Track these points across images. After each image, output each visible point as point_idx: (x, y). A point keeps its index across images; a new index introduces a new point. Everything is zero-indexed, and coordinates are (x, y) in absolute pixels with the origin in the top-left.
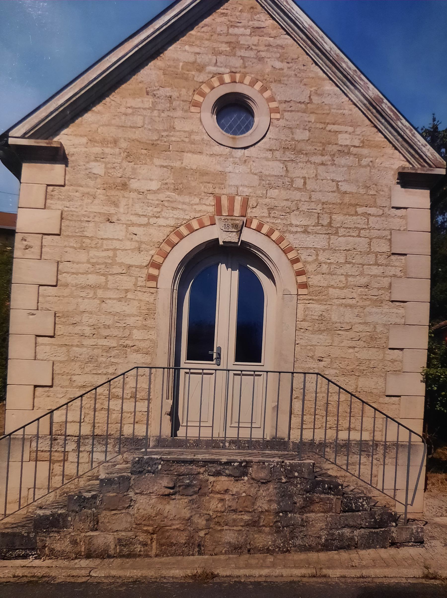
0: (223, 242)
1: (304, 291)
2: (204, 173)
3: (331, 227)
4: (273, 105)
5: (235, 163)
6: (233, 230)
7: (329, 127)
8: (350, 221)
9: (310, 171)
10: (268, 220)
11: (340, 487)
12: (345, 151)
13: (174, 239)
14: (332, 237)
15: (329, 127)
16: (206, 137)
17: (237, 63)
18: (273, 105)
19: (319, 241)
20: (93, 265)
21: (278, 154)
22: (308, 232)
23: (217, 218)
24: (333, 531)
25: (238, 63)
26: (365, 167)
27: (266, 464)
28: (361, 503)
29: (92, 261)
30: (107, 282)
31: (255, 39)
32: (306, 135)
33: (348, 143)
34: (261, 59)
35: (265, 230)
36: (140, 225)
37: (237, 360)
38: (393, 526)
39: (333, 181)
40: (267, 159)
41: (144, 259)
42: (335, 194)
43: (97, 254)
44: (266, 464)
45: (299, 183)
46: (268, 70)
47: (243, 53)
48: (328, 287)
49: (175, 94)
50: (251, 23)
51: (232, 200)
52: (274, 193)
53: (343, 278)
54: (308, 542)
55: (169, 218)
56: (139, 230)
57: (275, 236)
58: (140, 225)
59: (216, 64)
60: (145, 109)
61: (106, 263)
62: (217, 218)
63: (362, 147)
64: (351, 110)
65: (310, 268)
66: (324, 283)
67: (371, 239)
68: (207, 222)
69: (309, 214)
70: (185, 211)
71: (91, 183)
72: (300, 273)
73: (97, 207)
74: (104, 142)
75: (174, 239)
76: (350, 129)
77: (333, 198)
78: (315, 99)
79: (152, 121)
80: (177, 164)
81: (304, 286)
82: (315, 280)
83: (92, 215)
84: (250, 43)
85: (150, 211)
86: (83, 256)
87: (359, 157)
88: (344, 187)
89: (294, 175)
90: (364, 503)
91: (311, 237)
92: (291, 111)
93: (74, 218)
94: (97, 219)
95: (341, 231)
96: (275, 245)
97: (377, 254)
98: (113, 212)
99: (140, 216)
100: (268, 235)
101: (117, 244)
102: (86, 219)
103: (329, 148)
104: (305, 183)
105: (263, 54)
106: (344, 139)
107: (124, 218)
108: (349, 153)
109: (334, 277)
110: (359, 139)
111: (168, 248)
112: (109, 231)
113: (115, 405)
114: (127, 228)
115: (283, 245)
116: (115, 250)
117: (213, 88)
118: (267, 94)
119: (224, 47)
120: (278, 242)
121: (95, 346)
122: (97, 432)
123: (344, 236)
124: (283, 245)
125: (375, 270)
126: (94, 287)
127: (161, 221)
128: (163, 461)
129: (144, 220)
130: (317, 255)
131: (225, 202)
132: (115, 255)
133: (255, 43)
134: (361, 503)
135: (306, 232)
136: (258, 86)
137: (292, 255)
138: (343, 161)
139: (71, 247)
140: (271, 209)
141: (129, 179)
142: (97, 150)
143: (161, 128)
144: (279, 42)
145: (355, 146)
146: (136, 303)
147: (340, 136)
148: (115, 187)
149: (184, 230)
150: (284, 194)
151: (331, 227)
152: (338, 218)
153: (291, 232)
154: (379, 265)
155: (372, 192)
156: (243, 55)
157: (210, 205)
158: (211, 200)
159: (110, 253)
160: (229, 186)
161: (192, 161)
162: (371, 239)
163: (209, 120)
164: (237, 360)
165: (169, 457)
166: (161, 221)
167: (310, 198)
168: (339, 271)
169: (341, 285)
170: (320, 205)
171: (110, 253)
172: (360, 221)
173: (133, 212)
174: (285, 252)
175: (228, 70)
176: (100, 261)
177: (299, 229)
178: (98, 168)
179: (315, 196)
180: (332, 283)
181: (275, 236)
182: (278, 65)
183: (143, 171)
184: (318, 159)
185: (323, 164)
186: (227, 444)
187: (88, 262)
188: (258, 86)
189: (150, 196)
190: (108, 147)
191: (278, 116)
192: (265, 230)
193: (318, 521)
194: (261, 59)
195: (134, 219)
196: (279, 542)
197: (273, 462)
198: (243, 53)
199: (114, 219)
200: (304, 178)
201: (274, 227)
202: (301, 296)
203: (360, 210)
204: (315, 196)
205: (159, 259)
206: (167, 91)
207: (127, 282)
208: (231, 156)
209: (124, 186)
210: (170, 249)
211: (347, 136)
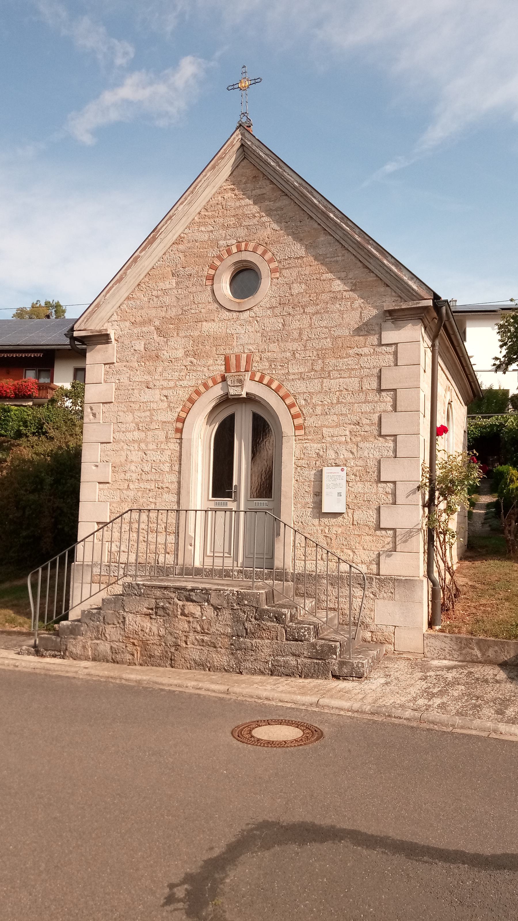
0: (247, 394)
1: (302, 432)
3: (324, 371)
4: (273, 265)
6: (238, 384)
11: (284, 616)
14: (325, 380)
18: (273, 265)
19: (315, 385)
24: (279, 658)
27: (222, 592)
28: (303, 633)
30: (146, 436)
38: (333, 658)
40: (269, 317)
44: (222, 592)
45: (296, 334)
48: (322, 426)
51: (238, 358)
54: (260, 666)
56: (169, 393)
64: (343, 256)
73: (140, 377)
74: (143, 323)
82: (310, 421)
90: (306, 633)
100: (268, 385)
101: (155, 406)
107: (157, 383)
110: (351, 283)
112: (147, 395)
113: (152, 537)
122: (140, 560)
125: (366, 408)
126: (139, 442)
127: (185, 383)
128: (145, 586)
131: (233, 361)
134: (303, 633)
148: (150, 358)
151: (324, 371)
153: (288, 380)
158: (221, 361)
164: (270, 497)
165: (149, 583)
166: (185, 383)
181: (274, 386)
185: (317, 313)
186: (236, 573)
191: (278, 275)
193: (265, 646)
195: (165, 384)
196: (233, 662)
197: (227, 590)
199: (151, 385)
202: (299, 437)
205: (183, 415)
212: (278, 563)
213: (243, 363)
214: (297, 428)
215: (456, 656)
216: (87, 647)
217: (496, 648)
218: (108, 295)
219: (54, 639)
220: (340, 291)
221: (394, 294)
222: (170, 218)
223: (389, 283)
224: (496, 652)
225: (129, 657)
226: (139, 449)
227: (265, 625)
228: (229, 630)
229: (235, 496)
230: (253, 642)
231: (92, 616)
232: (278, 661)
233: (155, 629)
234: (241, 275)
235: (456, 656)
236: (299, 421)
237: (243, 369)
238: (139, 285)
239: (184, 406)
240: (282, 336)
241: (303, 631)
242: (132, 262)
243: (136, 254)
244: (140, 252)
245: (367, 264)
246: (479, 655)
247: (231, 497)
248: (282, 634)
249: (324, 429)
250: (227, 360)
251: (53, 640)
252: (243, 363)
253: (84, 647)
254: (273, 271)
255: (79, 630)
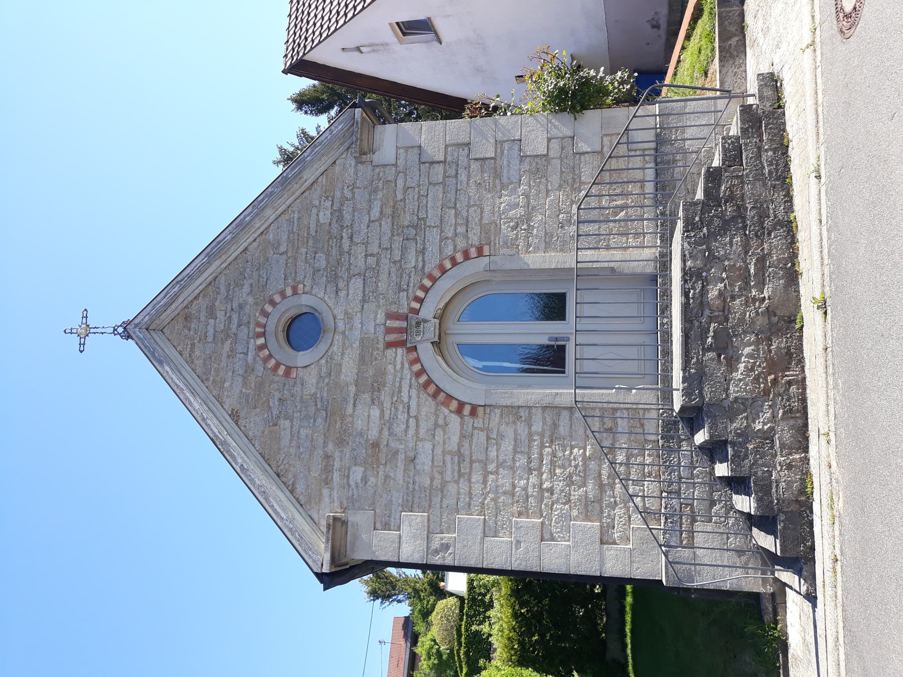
2: (362, 360)
4: (289, 292)
5: (351, 329)
7: (313, 232)
8: (411, 205)
9: (360, 251)
10: (410, 291)
12: (338, 214)
13: (432, 389)
15: (313, 232)
16: (323, 361)
17: (243, 333)
19: (433, 236)
20: (460, 475)
21: (341, 284)
22: (424, 249)
23: (409, 345)
25: (243, 333)
26: (353, 193)
29: (456, 478)
30: (479, 461)
31: (220, 315)
32: (321, 256)
33: (328, 213)
34: (241, 307)
35: (421, 294)
36: (417, 425)
37: (564, 319)
39: (368, 226)
41: (454, 420)
42: (383, 223)
43: (449, 473)
46: (251, 300)
47: (234, 326)
48: (481, 225)
49: (277, 395)
50: (202, 319)
51: (389, 331)
52: (382, 286)
53: (472, 210)
55: (410, 393)
57: (427, 283)
58: (417, 425)
59: (246, 354)
60: (292, 428)
61: (459, 462)
62: (409, 345)
63: (333, 197)
64: (294, 212)
65: (461, 244)
66: (477, 229)
67: (430, 184)
68: (413, 355)
69: (404, 250)
70: (401, 379)
71: (372, 480)
72: (467, 256)
74: (328, 469)
75: (432, 389)
76: (314, 211)
77: (386, 225)
78: (282, 249)
79: (307, 417)
80: (353, 389)
81: (480, 253)
82: (474, 239)
83: (407, 479)
84: (223, 319)
85: (402, 417)
86: (452, 488)
87: (344, 199)
88: (375, 213)
89: (363, 267)
91: (427, 246)
92: (296, 273)
93: (410, 498)
94: (412, 474)
95: (421, 215)
96: (438, 283)
97: (445, 177)
98: (403, 456)
99: (407, 427)
100: (426, 290)
101: (439, 451)
102: (411, 486)
103: (335, 231)
104: (371, 255)
105: (235, 305)
106: (325, 217)
108: (340, 211)
109: (470, 219)
111: (442, 395)
112: (425, 461)
114: (421, 440)
115: (437, 273)
116: (444, 453)
117: (270, 356)
118: (277, 298)
119: (227, 346)
120: (434, 280)
121: (552, 474)
123: (427, 211)
124: (437, 273)
127: (413, 404)
129: (412, 422)
130: (447, 238)
131: (392, 337)
132: (450, 452)
133: (223, 313)
135: (423, 252)
136: (269, 308)
137: (448, 265)
138: (347, 217)
139: (441, 501)
140: (400, 290)
141: (367, 440)
142: (336, 476)
143: (314, 408)
144: (223, 289)
145: (332, 205)
146: (503, 427)
147: (322, 221)
149: (423, 379)
150: (384, 276)
152: (407, 219)
154: (457, 173)
155: (380, 185)
156: (235, 326)
157: (396, 353)
158: (390, 352)
159: (448, 458)
160: (375, 333)
161: (349, 370)
162: (430, 184)
163: (302, 358)
164: (564, 319)
167: (387, 249)
168: (465, 214)
169: (479, 211)
170: (395, 238)
171: (448, 458)
172: (412, 195)
173: (404, 434)
174: (444, 271)
175: (252, 340)
176: (457, 469)
177: (420, 259)
178: (357, 473)
179: (386, 244)
180: (477, 220)
181: (427, 283)
182: (246, 289)
183: (359, 424)
184: (346, 243)
185: (351, 238)
187: (457, 482)
188: (269, 308)
189: (387, 417)
190: (333, 465)
191: (301, 286)
192: (421, 294)
194: (241, 307)
195: (411, 432)
198: (234, 326)
199: (411, 454)
200: (366, 256)
201: (419, 285)
203: (400, 196)
204: (386, 244)
205: (454, 405)
206: (274, 403)
207: (480, 438)
208: (343, 333)
209: (376, 445)
210: (442, 394)
211: (321, 214)
212: (650, 269)
213: (396, 324)
214: (480, 253)
215: (741, 61)
216: (788, 461)
217: (726, 23)
218: (283, 515)
219: (782, 525)
220: (331, 213)
221: (344, 156)
222: (204, 419)
223: (330, 161)
224: (730, 24)
225: (793, 389)
226: (496, 473)
227: (725, 192)
228: (737, 239)
229: (563, 339)
230: (749, 206)
231: (739, 456)
232: (770, 172)
233: (748, 350)
234: (291, 334)
235: (741, 61)
236: (473, 252)
237: (404, 324)
238: (278, 475)
239: (443, 404)
240: (369, 275)
241: (727, 146)
242: (246, 475)
243: (238, 470)
244: (237, 463)
245: (307, 184)
246: (737, 38)
247: (564, 346)
248: (734, 171)
249: (485, 221)
250: (389, 345)
251: (784, 528)
252: (396, 324)
253: (789, 467)
254: (295, 292)
255: (763, 479)
